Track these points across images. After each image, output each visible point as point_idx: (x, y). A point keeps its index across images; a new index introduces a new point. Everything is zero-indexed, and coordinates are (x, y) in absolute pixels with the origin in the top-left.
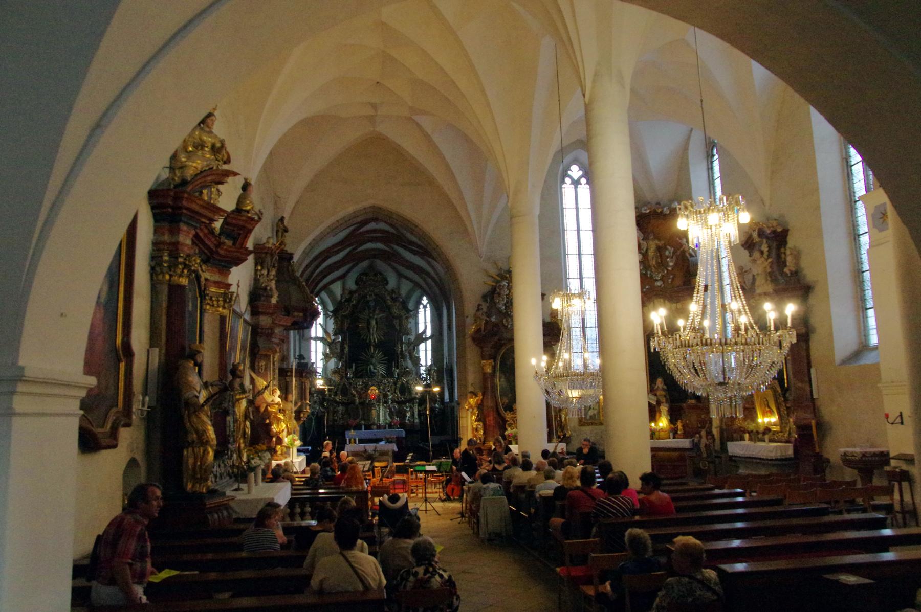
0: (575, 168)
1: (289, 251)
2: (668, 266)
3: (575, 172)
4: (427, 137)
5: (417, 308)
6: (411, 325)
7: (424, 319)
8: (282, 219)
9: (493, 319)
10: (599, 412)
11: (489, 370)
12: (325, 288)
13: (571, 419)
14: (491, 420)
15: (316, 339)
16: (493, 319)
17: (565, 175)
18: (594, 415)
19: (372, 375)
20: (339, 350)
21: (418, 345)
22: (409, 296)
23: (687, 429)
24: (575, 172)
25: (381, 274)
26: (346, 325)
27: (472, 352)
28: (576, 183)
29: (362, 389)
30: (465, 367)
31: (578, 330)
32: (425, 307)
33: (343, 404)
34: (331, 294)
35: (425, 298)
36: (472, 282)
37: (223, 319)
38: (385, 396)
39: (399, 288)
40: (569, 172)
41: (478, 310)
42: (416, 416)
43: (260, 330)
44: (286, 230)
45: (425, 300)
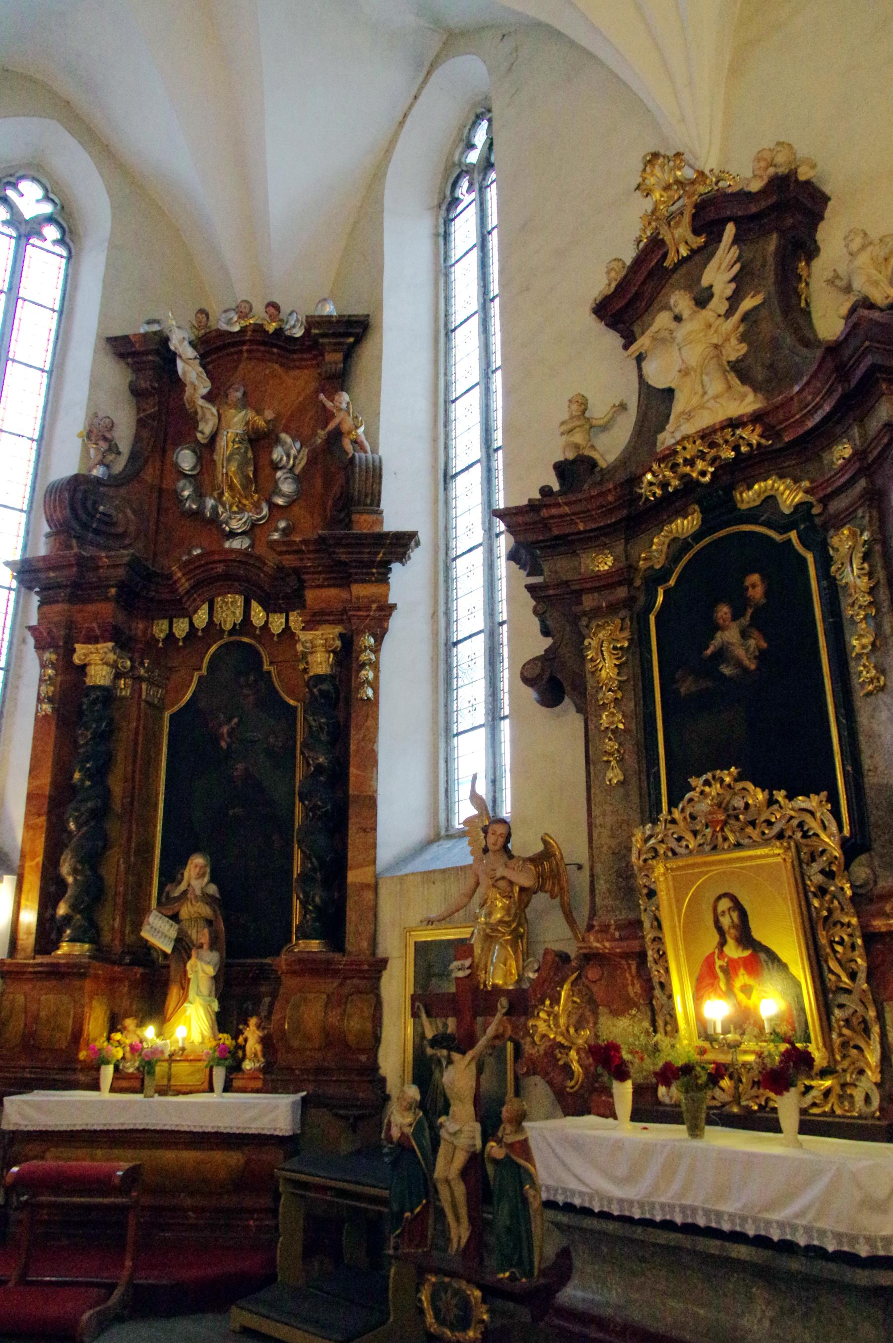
2: (277, 492)
23: (283, 1058)
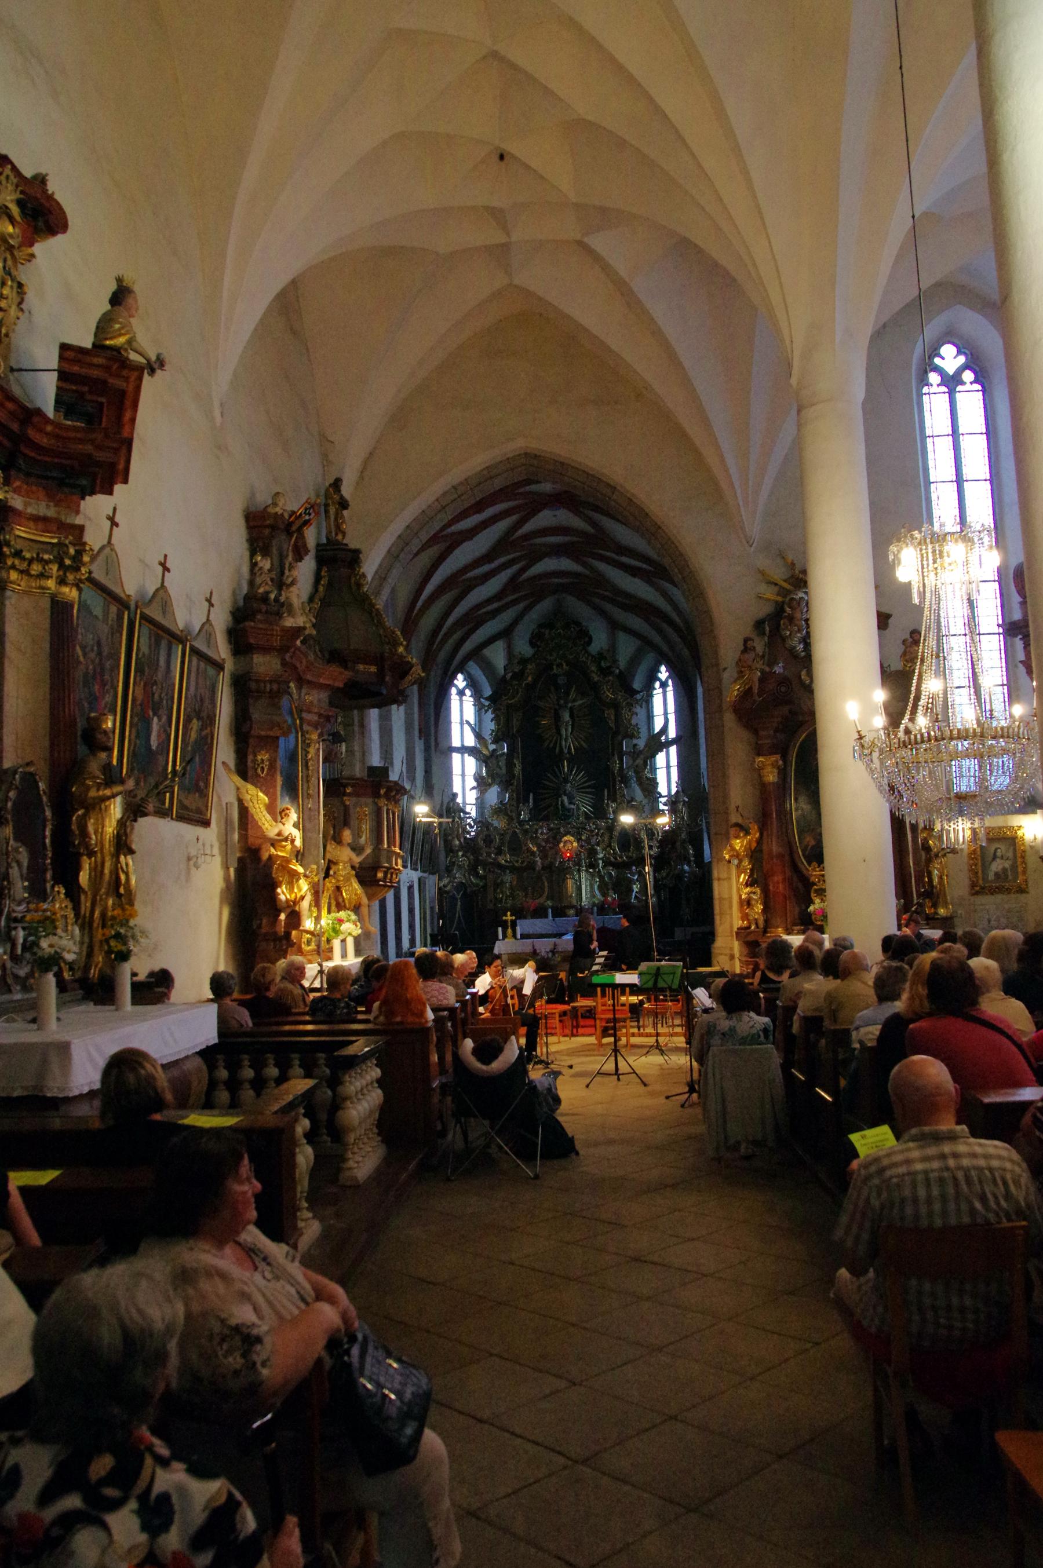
0: (948, 350)
1: (353, 546)
3: (950, 359)
4: (623, 289)
5: (649, 688)
6: (639, 719)
7: (663, 707)
8: (337, 484)
9: (778, 669)
10: (1014, 867)
11: (771, 777)
12: (476, 654)
13: (952, 879)
14: (778, 883)
15: (463, 750)
16: (778, 669)
17: (928, 366)
18: (1005, 870)
19: (565, 815)
20: (504, 771)
21: (653, 756)
22: (635, 661)
24: (950, 359)
25: (578, 624)
26: (516, 723)
27: (737, 743)
28: (952, 382)
29: (547, 841)
30: (725, 776)
31: (965, 691)
32: (664, 685)
33: (513, 869)
34: (488, 667)
35: (663, 668)
36: (732, 601)
37: (60, 610)
38: (592, 853)
39: (613, 648)
40: (937, 361)
41: (746, 650)
42: (650, 891)
43: (253, 685)
44: (344, 504)
45: (663, 674)
